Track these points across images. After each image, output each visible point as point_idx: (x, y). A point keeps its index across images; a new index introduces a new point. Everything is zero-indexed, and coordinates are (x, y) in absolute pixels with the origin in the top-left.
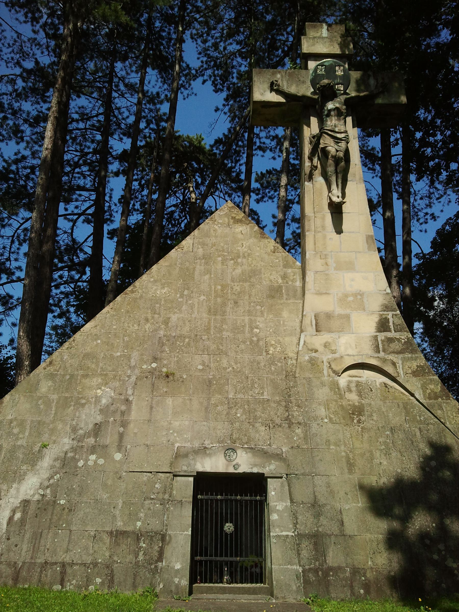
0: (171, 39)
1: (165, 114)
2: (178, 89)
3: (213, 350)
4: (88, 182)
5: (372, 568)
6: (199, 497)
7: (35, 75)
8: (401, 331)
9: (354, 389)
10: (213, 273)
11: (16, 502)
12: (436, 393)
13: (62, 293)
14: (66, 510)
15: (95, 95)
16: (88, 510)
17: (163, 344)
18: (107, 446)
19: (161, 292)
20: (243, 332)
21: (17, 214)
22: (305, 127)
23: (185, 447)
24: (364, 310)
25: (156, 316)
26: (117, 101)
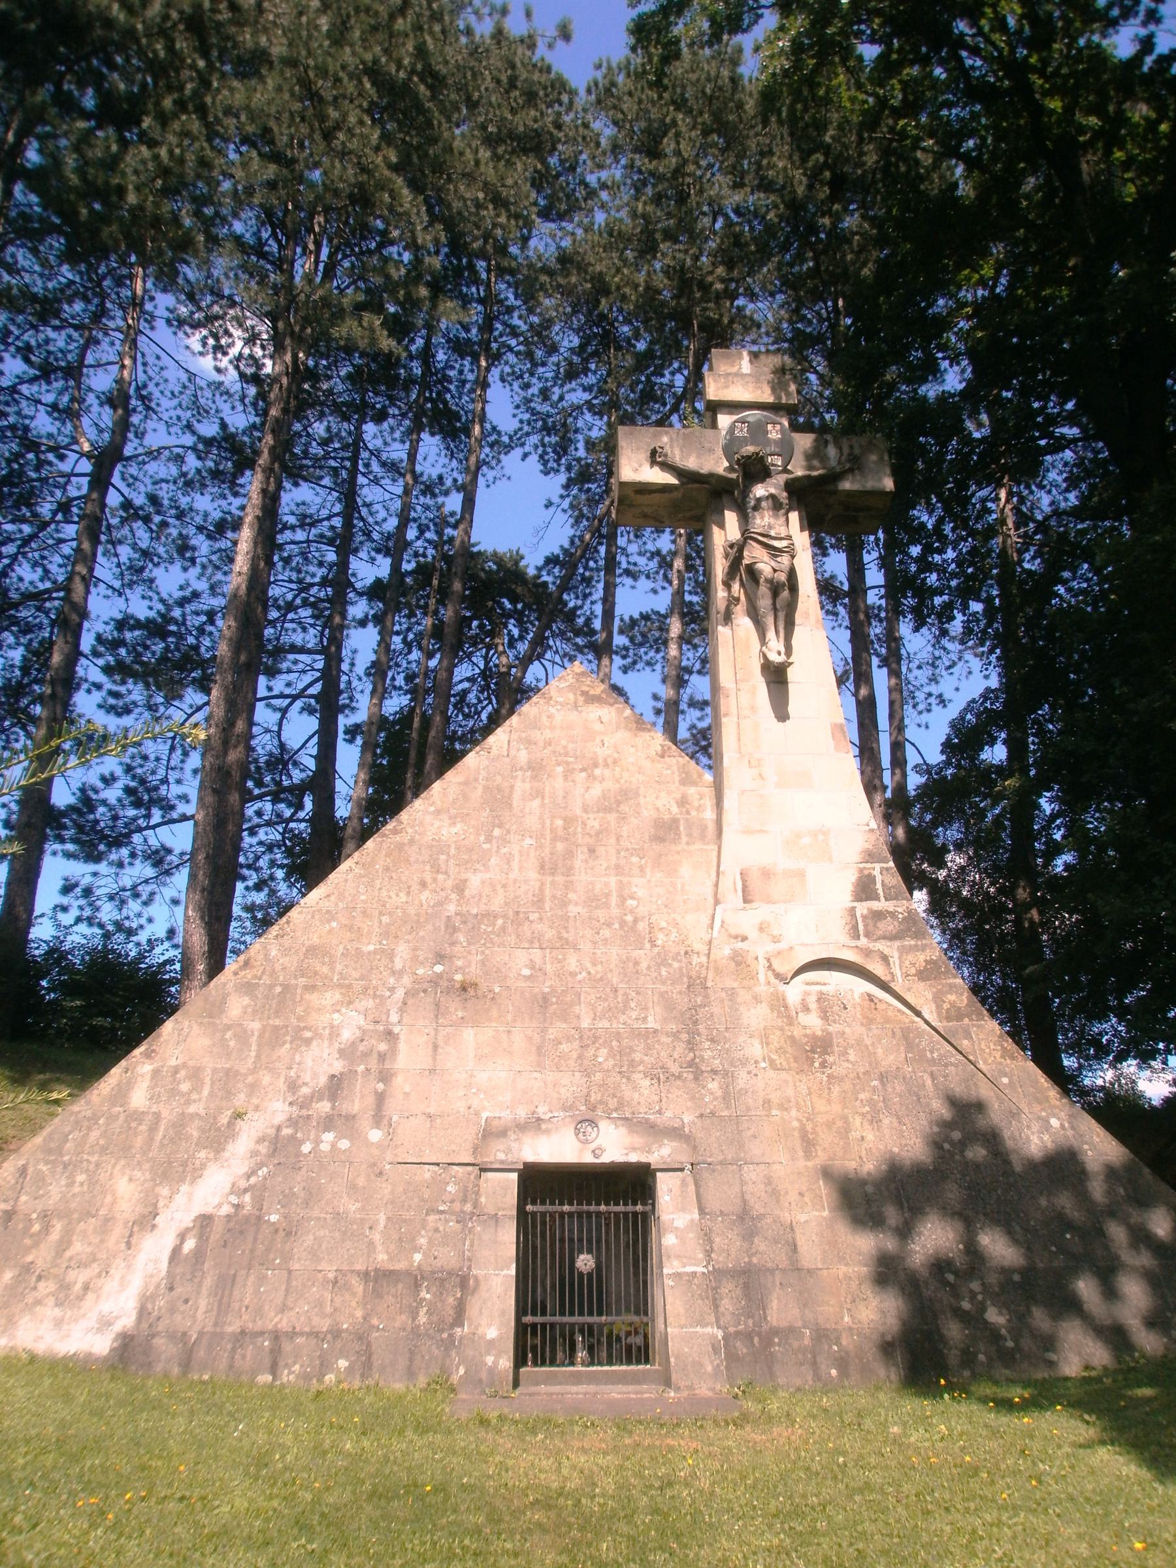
0: (464, 382)
1: (452, 514)
2: (478, 468)
4: (311, 638)
6: (529, 1208)
7: (219, 447)
9: (813, 1006)
11: (187, 1220)
13: (261, 843)
14: (282, 1233)
15: (327, 481)
17: (455, 930)
19: (449, 831)
20: (607, 905)
21: (181, 697)
22: (716, 529)
25: (441, 877)
26: (365, 491)
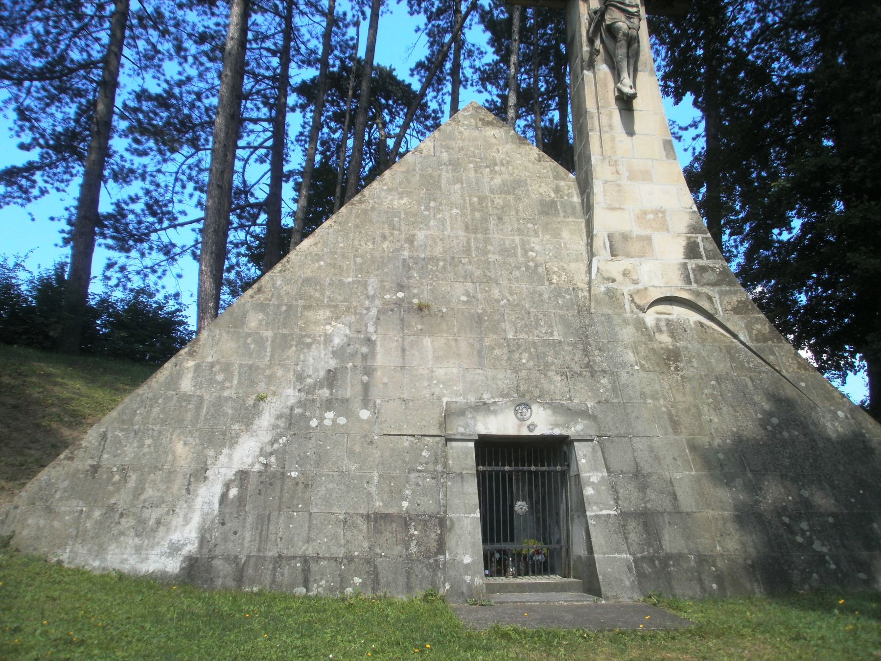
3: (478, 277)
5: (722, 555)
8: (714, 258)
9: (664, 329)
10: (464, 182)
11: (230, 474)
12: (764, 334)
14: (301, 486)
16: (331, 486)
17: (410, 268)
18: (347, 400)
19: (400, 203)
23: (456, 402)
24: (668, 230)
25: (396, 232)
